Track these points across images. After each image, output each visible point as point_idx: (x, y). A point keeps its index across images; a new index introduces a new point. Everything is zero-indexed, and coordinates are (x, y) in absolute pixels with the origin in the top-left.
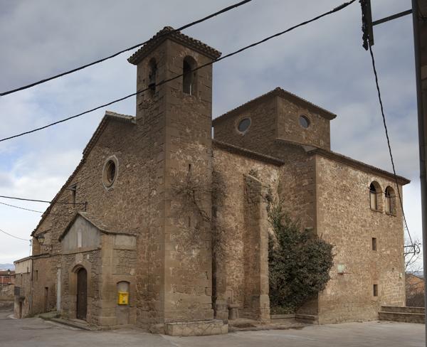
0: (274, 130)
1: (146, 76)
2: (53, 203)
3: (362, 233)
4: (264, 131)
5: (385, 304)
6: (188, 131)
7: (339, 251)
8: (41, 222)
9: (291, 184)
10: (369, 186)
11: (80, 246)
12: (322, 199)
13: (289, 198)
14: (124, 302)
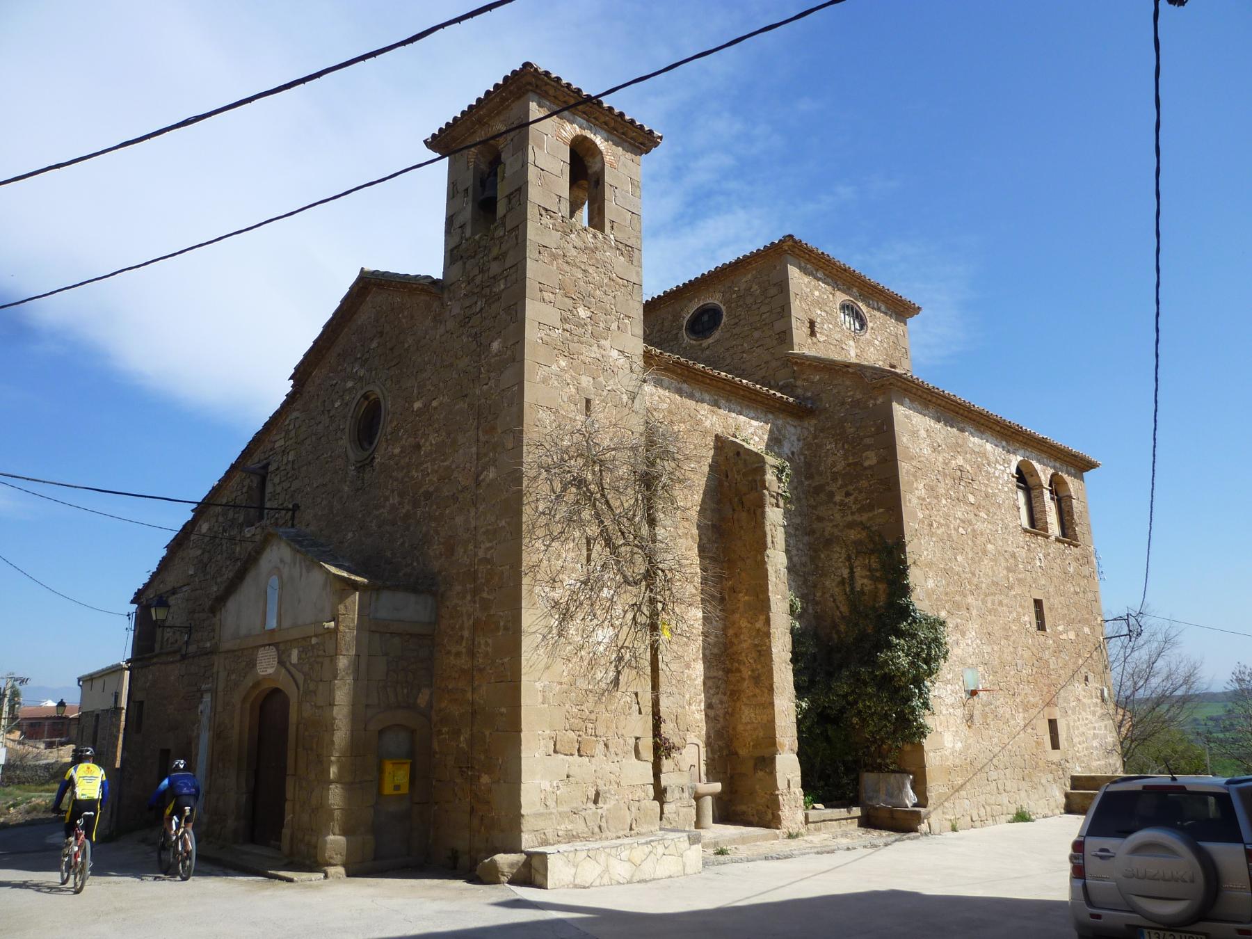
0: (784, 332)
1: (468, 180)
2: (202, 509)
3: (1010, 588)
4: (756, 334)
5: (1078, 771)
6: (583, 313)
7: (963, 634)
8: (164, 564)
9: (834, 465)
10: (1014, 471)
11: (272, 623)
12: (915, 501)
13: (831, 495)
14: (397, 787)
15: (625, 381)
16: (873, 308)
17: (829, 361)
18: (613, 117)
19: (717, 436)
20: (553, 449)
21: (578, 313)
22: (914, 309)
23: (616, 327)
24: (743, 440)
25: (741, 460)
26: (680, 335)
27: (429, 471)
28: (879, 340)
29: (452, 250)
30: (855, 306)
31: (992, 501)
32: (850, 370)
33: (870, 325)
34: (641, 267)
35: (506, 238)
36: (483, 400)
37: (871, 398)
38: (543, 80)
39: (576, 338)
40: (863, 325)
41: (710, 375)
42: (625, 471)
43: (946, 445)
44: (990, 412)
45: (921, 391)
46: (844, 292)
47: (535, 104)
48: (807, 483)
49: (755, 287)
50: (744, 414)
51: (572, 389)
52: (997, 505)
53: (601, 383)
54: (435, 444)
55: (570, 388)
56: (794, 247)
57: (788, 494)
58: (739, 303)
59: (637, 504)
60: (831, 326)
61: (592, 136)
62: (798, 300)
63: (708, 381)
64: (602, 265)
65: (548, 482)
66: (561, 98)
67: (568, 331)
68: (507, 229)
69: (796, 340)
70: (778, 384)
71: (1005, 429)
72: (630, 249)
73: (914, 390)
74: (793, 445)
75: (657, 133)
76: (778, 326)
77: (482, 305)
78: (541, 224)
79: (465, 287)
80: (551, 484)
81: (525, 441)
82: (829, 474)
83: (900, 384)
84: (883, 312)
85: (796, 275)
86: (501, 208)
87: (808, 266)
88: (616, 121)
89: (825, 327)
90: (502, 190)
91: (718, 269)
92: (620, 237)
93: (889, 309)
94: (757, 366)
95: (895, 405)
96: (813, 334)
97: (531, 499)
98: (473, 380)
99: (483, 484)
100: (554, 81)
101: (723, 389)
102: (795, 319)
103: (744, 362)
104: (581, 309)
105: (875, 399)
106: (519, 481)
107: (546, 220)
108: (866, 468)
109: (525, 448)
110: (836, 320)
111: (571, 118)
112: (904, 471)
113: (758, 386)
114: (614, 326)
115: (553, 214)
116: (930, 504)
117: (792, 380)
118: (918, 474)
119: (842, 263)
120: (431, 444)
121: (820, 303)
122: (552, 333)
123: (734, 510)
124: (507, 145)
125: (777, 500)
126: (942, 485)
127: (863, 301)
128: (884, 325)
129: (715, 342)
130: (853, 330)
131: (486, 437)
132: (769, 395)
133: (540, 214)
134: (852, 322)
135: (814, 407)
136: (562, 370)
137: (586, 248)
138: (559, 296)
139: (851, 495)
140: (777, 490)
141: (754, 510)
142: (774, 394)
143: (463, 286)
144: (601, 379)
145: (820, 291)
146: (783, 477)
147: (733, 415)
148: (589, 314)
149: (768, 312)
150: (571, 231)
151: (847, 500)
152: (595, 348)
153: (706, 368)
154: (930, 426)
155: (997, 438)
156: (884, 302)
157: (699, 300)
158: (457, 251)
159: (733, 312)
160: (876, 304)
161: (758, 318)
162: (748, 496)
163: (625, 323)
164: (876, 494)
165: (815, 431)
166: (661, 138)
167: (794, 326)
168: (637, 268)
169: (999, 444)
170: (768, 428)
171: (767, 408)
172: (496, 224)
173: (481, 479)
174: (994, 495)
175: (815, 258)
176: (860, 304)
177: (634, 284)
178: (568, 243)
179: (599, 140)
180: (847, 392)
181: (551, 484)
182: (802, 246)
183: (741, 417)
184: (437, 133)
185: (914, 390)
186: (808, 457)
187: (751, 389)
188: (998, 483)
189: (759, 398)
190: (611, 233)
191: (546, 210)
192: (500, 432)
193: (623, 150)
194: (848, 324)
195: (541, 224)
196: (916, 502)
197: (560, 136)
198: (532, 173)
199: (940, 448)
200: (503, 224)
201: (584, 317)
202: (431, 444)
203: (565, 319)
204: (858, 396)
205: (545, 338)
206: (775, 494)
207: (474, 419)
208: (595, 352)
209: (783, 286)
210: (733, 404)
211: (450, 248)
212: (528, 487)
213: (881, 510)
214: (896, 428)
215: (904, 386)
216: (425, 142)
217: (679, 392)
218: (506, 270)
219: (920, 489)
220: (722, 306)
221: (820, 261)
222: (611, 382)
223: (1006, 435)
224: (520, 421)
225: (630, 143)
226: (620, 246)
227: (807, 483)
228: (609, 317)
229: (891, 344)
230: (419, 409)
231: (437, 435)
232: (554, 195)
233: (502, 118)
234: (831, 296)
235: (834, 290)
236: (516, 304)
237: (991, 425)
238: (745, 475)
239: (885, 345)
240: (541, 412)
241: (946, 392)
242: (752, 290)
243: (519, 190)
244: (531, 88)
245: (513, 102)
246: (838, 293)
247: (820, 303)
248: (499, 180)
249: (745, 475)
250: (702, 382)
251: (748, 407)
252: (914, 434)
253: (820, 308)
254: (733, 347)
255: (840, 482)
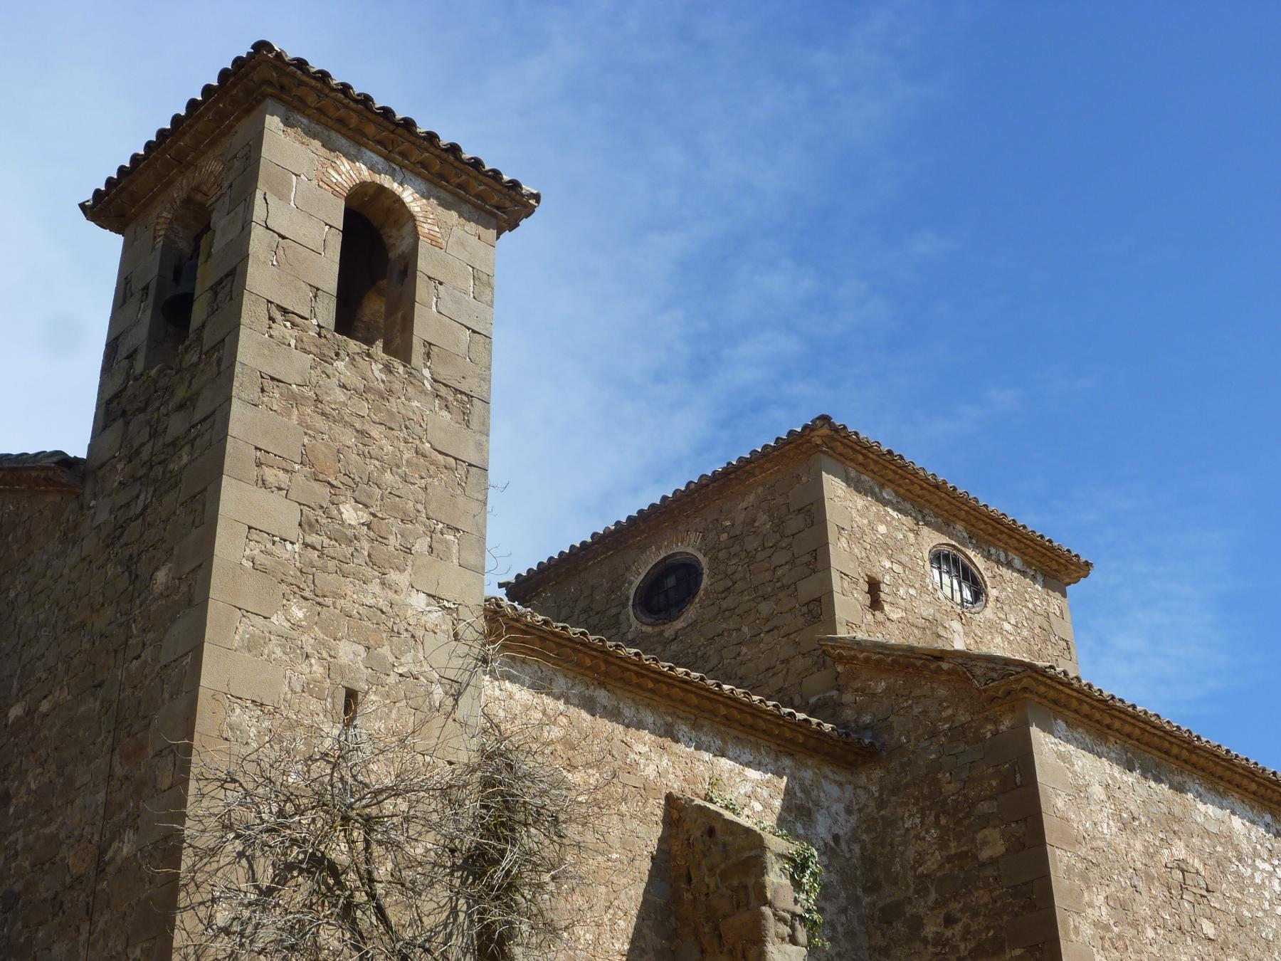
0: (818, 600)
1: (151, 269)
4: (765, 608)
6: (351, 514)
9: (920, 861)
12: (1088, 931)
13: (916, 924)
15: (441, 659)
16: (998, 562)
17: (903, 650)
18: (438, 152)
19: (669, 798)
20: (261, 790)
21: (341, 514)
22: (1078, 564)
23: (426, 548)
24: (727, 807)
25: (716, 844)
26: (622, 617)
27: (19, 848)
28: (1013, 622)
29: (109, 402)
30: (961, 557)
31: (1252, 935)
32: (945, 666)
33: (993, 593)
34: (488, 435)
35: (202, 366)
36: (129, 691)
37: (987, 719)
38: (293, 76)
39: (331, 565)
40: (978, 592)
41: (654, 671)
42: (430, 846)
43: (1148, 817)
44: (1233, 753)
45: (1090, 705)
46: (938, 529)
47: (276, 119)
48: (868, 900)
49: (763, 518)
50: (730, 754)
51: (315, 668)
52: (1263, 943)
53: (385, 657)
54: (36, 792)
55: (311, 665)
56: (833, 439)
57: (816, 916)
58: (733, 551)
59: (455, 920)
60: (912, 591)
61: (395, 187)
62: (843, 540)
63: (651, 685)
64: (405, 425)
65: (244, 862)
66: (331, 111)
67: (314, 548)
68: (205, 348)
69: (840, 614)
70: (808, 703)
71: (1267, 788)
72: (465, 398)
73: (1075, 704)
74: (836, 822)
75: (527, 188)
76: (807, 590)
77: (146, 499)
78: (271, 336)
79: (123, 469)
80: (251, 867)
81: (194, 770)
82: (910, 880)
83: (1042, 689)
84: (1019, 571)
85: (840, 492)
86: (199, 312)
87: (864, 477)
88: (443, 161)
89: (902, 592)
90: (206, 276)
91: (693, 486)
92: (444, 373)
93: (1029, 565)
94: (767, 670)
95: (1036, 732)
96: (876, 604)
97: (197, 898)
98: (116, 651)
99: (110, 869)
100: (315, 78)
101: (683, 702)
102: (838, 574)
103: (742, 663)
104: (348, 506)
105: (996, 722)
106: (174, 857)
107: (282, 329)
108: (983, 865)
109: (193, 786)
110: (923, 580)
111: (353, 151)
112: (1061, 867)
113: (756, 698)
114: (421, 546)
115: (297, 320)
116: (1120, 937)
117: (834, 693)
118: (1091, 875)
119: (929, 473)
120: (29, 792)
121: (888, 548)
122: (277, 550)
123: (703, 952)
124: (221, 196)
125: (793, 927)
126: (1145, 898)
127: (976, 547)
128: (1022, 595)
129: (688, 626)
130: (959, 601)
131: (127, 767)
132: (780, 717)
133: (271, 318)
134: (956, 586)
135: (877, 744)
136: (295, 626)
137: (367, 389)
138: (300, 478)
139: (956, 921)
140: (791, 906)
141: (744, 951)
142: (791, 714)
143: (119, 467)
144: (385, 650)
145: (887, 524)
146: (804, 880)
147: (707, 756)
148: (365, 517)
149: (786, 563)
150: (337, 354)
151: (948, 933)
152: (375, 587)
153: (644, 657)
154: (1113, 777)
155: (1252, 808)
156: (1023, 554)
157: (659, 549)
158: (118, 404)
159: (722, 567)
160: (1002, 554)
161: (768, 576)
162: (730, 920)
163: (446, 541)
164: (1006, 918)
165: (881, 794)
166: (537, 197)
167: (836, 586)
168: (478, 437)
169: (1256, 819)
170: (783, 785)
171: (779, 745)
172: (187, 343)
173: (107, 858)
174: (1255, 921)
175: (876, 462)
176: (971, 553)
177: (470, 465)
178: (328, 377)
179: (408, 195)
180: (940, 712)
181: (251, 867)
182: (847, 436)
183: (723, 761)
184: (103, 188)
185: (1075, 704)
186: (869, 846)
187: (741, 703)
188: (1262, 897)
189: (762, 724)
190: (425, 366)
191: (285, 311)
192: (151, 753)
193: (460, 216)
194: (947, 591)
195: (271, 336)
196: (1088, 932)
197: (325, 179)
198: (259, 241)
199: (1137, 823)
200: (199, 339)
201: (353, 523)
202: (29, 792)
203: (310, 525)
204: (963, 717)
205: (261, 559)
206: (788, 916)
207: (109, 732)
208: (374, 594)
209: (814, 513)
210: (706, 734)
211: (107, 397)
212: (192, 870)
213: (1018, 952)
214: (1041, 778)
215: (1052, 694)
216: (82, 206)
217: (590, 706)
218: (194, 426)
219: (1098, 906)
220: (700, 557)
221: (885, 468)
222: (408, 657)
223: (1270, 800)
224: (188, 727)
225: (475, 206)
226: (443, 391)
227: (868, 900)
228: (410, 526)
229: (1037, 630)
230: (18, 719)
231: (40, 770)
232: (303, 285)
233: (218, 151)
234: (911, 535)
235: (917, 524)
236: (204, 490)
237: (1237, 778)
238: (724, 876)
239: (1025, 633)
240: (238, 711)
241: (1139, 708)
242: (757, 524)
243: (232, 273)
244: (269, 90)
245: (238, 119)
246: (925, 531)
247: (888, 548)
248: (201, 260)
249: (724, 876)
250: (638, 685)
251: (738, 740)
252: (1080, 791)
253: (890, 557)
254: (722, 634)
255: (933, 896)
